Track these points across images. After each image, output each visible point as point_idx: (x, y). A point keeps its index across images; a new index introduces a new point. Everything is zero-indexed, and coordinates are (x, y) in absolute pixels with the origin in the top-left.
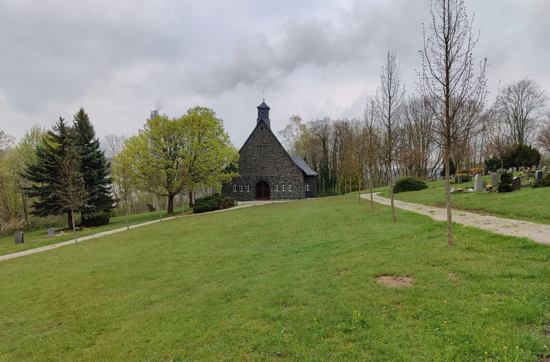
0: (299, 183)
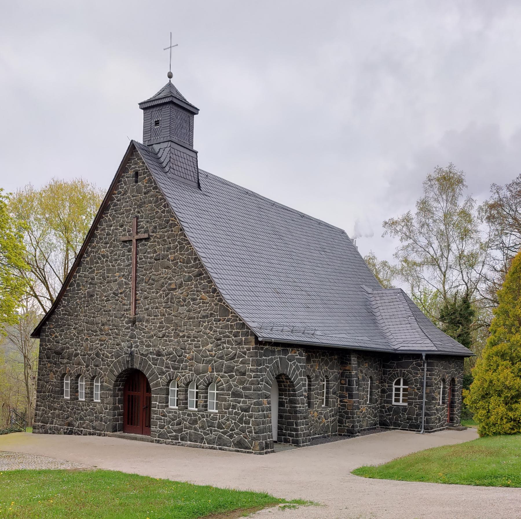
0: (242, 382)
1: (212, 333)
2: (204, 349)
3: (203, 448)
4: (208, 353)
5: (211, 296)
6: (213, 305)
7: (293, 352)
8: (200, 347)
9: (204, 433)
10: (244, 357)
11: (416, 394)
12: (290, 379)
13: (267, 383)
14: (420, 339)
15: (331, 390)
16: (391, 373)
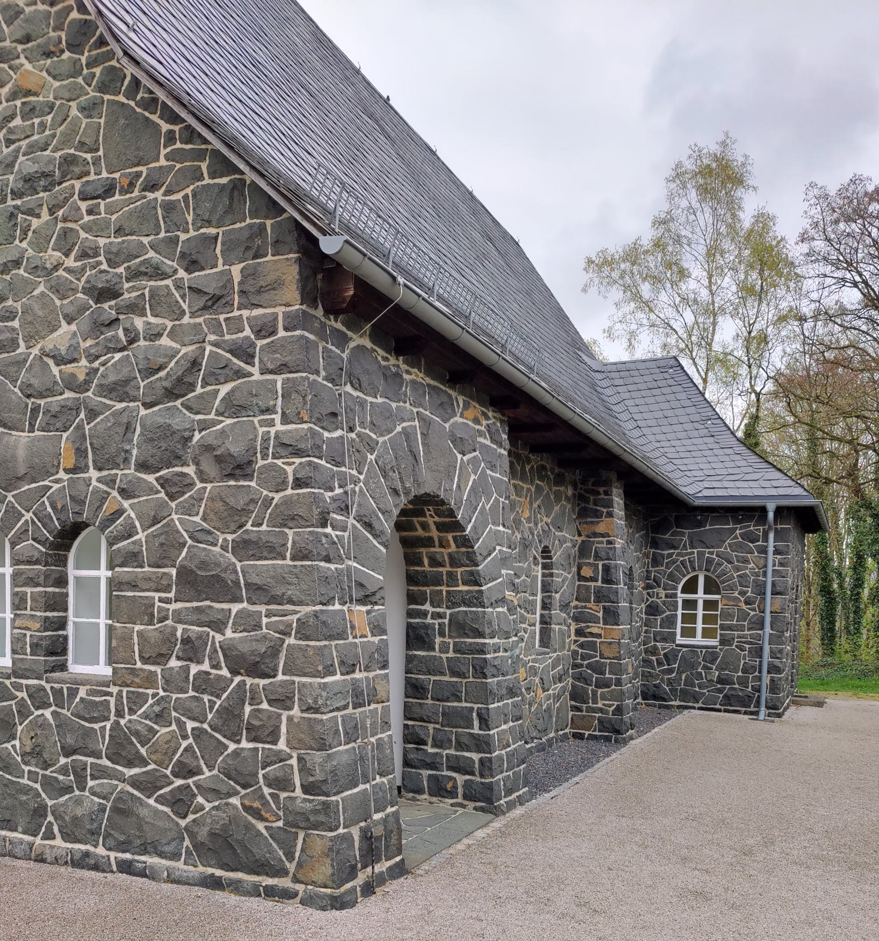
0: (233, 515)
1: (70, 262)
2: (35, 351)
3: (40, 859)
4: (55, 370)
5: (65, 69)
6: (74, 112)
7: (470, 413)
8: (14, 344)
9: (49, 784)
10: (240, 374)
11: (743, 616)
12: (457, 526)
13: (368, 526)
14: (750, 470)
15: (558, 596)
16: (674, 562)
